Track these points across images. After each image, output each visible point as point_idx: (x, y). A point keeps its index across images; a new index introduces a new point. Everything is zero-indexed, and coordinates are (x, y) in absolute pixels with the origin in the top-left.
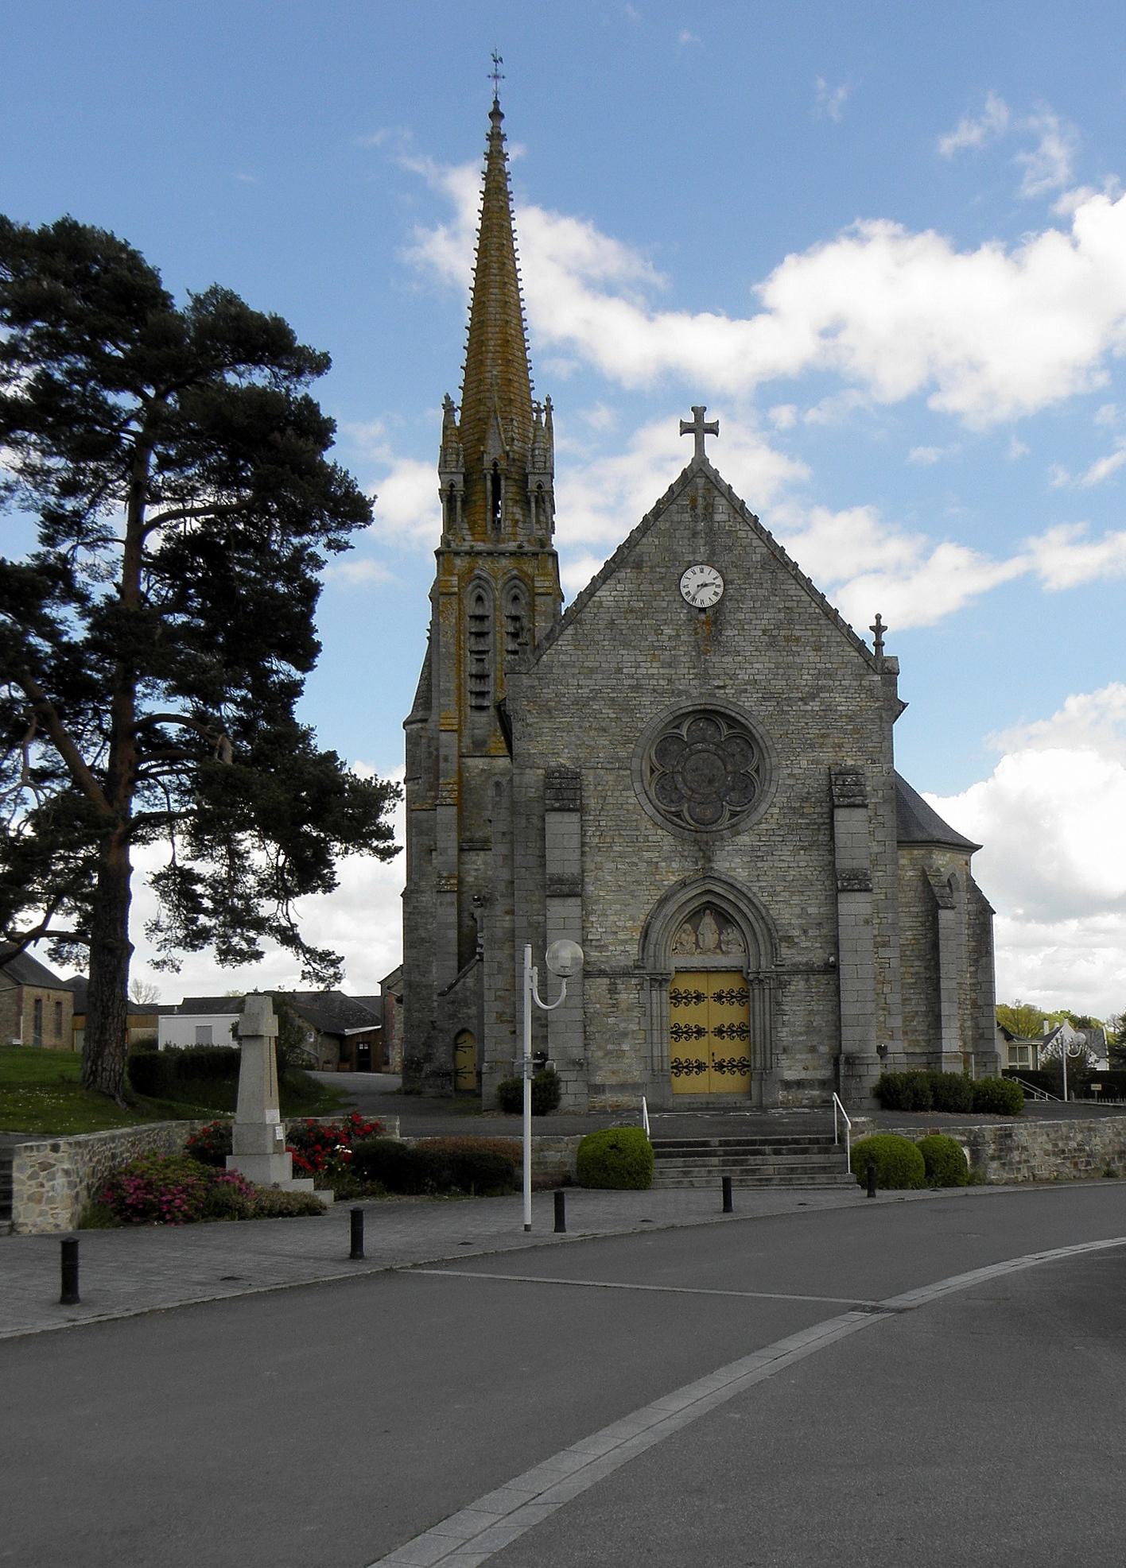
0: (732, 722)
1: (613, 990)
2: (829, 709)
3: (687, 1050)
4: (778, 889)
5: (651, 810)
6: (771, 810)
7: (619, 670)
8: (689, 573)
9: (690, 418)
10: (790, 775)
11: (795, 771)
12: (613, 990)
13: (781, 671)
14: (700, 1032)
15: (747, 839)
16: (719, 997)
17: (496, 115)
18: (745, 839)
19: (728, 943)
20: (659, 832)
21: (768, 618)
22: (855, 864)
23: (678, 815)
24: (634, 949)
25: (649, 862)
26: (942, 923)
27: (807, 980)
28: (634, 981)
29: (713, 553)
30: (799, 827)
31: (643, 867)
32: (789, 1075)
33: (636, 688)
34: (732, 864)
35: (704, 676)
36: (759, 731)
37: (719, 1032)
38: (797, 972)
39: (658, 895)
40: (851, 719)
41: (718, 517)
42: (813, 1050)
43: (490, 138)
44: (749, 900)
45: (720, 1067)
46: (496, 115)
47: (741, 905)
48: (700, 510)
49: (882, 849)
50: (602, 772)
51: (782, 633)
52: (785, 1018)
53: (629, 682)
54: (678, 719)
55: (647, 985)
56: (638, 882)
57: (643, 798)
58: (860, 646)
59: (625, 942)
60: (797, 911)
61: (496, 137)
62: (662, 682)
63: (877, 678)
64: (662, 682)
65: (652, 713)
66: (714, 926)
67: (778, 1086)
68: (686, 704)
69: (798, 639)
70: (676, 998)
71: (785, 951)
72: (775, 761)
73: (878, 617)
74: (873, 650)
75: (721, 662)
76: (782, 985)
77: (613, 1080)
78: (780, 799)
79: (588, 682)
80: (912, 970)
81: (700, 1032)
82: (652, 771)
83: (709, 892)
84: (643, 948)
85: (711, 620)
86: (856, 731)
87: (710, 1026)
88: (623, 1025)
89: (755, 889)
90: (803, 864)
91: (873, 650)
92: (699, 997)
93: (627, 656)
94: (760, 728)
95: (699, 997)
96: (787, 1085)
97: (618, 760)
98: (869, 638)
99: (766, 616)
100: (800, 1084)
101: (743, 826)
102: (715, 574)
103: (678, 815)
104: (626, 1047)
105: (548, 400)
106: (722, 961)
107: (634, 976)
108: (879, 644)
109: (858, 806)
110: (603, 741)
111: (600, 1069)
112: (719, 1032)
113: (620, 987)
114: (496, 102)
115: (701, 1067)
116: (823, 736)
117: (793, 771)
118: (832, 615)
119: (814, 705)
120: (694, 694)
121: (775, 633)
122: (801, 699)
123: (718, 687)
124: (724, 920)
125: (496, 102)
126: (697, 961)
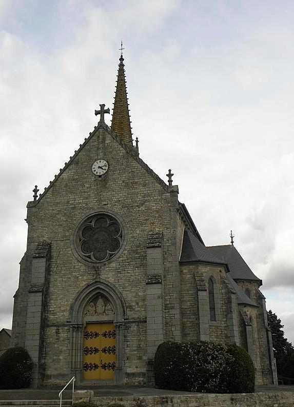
0: (111, 218)
1: (58, 332)
2: (149, 209)
3: (91, 359)
4: (126, 285)
5: (76, 255)
6: (124, 252)
7: (68, 202)
8: (95, 163)
9: (99, 109)
10: (133, 237)
11: (135, 235)
12: (58, 332)
13: (129, 196)
14: (96, 351)
15: (114, 265)
16: (105, 335)
17: (122, 59)
18: (113, 265)
19: (108, 310)
20: (79, 264)
21: (125, 176)
22: (156, 272)
23: (89, 257)
24: (66, 314)
25: (75, 277)
26: (200, 298)
27: (138, 325)
28: (66, 328)
29: (105, 155)
30: (136, 258)
31: (72, 279)
32: (129, 370)
33: (73, 208)
34: (108, 275)
35: (100, 201)
36: (120, 220)
37: (104, 351)
38: (134, 322)
39: (77, 290)
40: (157, 212)
41: (107, 142)
42: (140, 358)
43: (120, 66)
44: (114, 291)
45: (104, 367)
46: (122, 59)
47: (111, 293)
48: (100, 140)
49: (171, 265)
50: (59, 242)
51: (130, 181)
52: (128, 343)
53: (71, 206)
54: (90, 218)
55: (71, 329)
56: (70, 286)
57: (74, 251)
58: (161, 182)
59: (63, 311)
60: (134, 294)
61: (121, 66)
62: (83, 205)
63: (168, 194)
64: (83, 205)
65: (80, 217)
66: (103, 303)
67: (124, 375)
68: (92, 212)
69: (136, 183)
70: (87, 335)
71: (128, 313)
72: (126, 232)
73: (170, 171)
74: (168, 184)
75: (106, 194)
76: (127, 328)
77: (55, 373)
78: (128, 247)
79: (56, 208)
80: (190, 320)
81: (96, 351)
82: (80, 240)
83: (98, 288)
84: (71, 314)
85: (103, 179)
86: (160, 216)
87: (100, 348)
88: (60, 348)
89: (117, 286)
90: (137, 274)
91: (168, 184)
92: (97, 335)
93: (71, 197)
94: (121, 219)
95: (97, 335)
96: (128, 375)
97: (66, 236)
98: (166, 180)
99: (124, 175)
100: (134, 375)
101: (113, 259)
102: (105, 162)
103: (89, 257)
104: (61, 358)
105: (137, 138)
106: (105, 318)
107: (66, 326)
108: (170, 181)
109: (157, 247)
110: (60, 230)
111: (50, 368)
112: (104, 351)
113: (61, 331)
114: (122, 56)
115: (96, 367)
116: (146, 220)
117: (133, 235)
118: (150, 172)
119: (143, 208)
120: (94, 207)
121: (128, 181)
122: (137, 206)
123: (105, 205)
124: (107, 300)
125: (122, 56)
126: (94, 319)
